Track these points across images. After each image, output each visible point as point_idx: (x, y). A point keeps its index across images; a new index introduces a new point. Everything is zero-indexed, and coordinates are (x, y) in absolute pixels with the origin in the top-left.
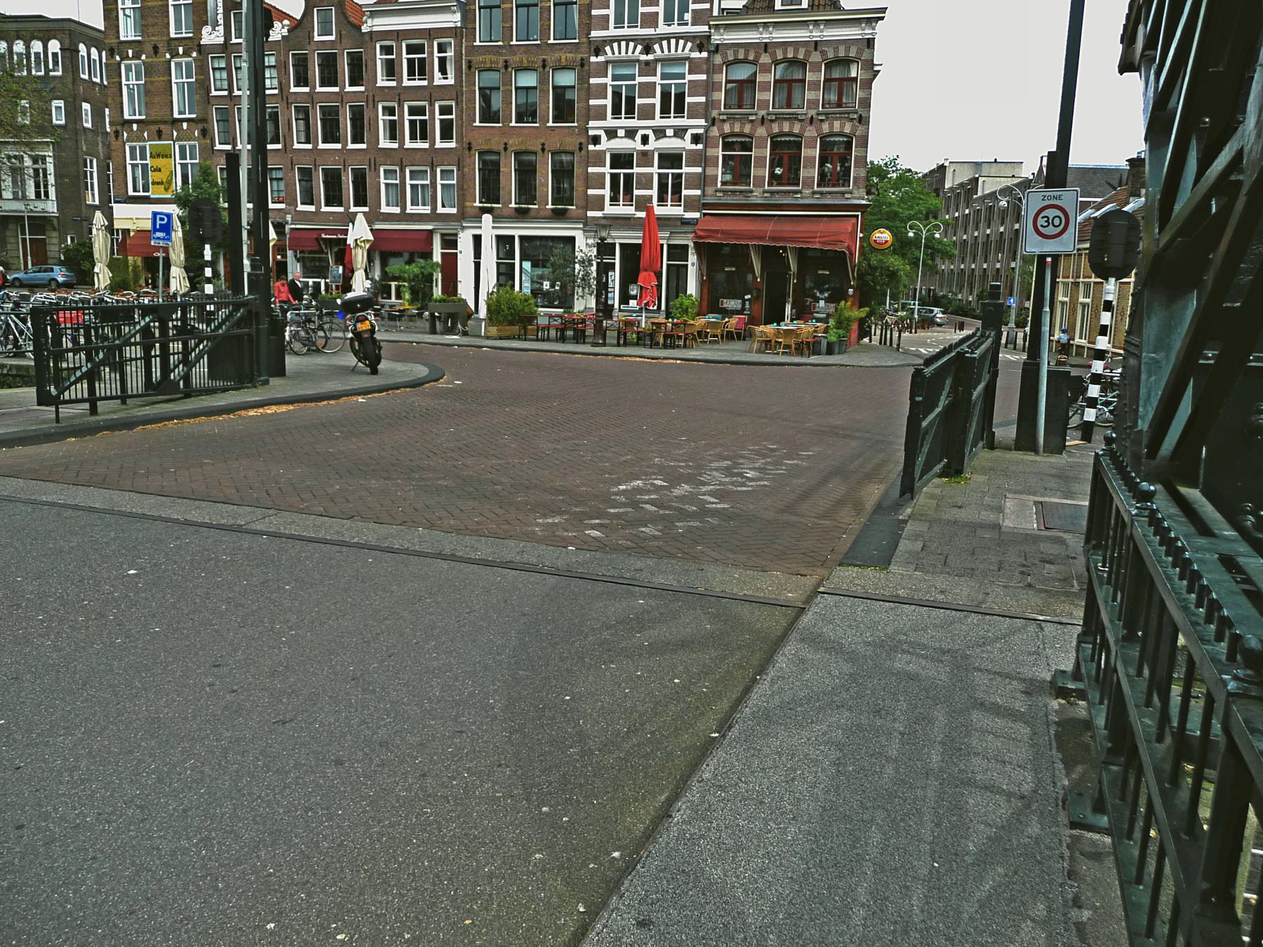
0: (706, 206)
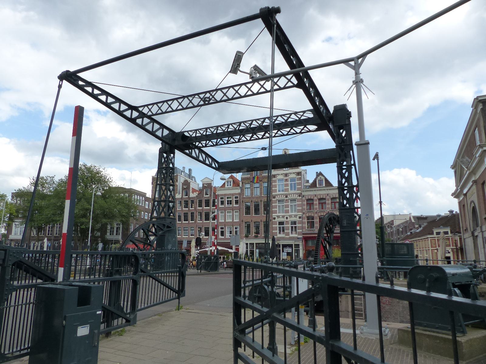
0: (303, 234)
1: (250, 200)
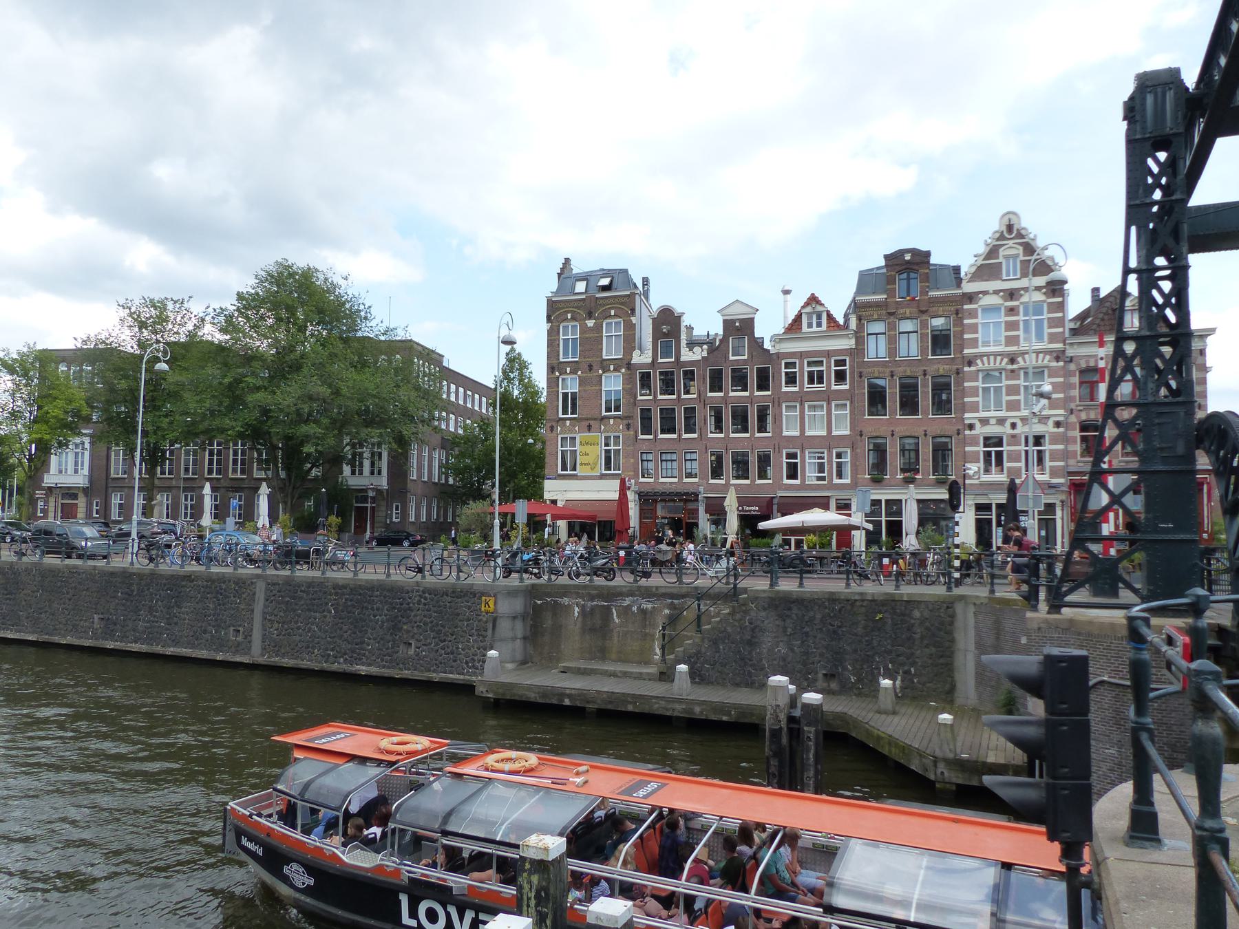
1: (888, 370)
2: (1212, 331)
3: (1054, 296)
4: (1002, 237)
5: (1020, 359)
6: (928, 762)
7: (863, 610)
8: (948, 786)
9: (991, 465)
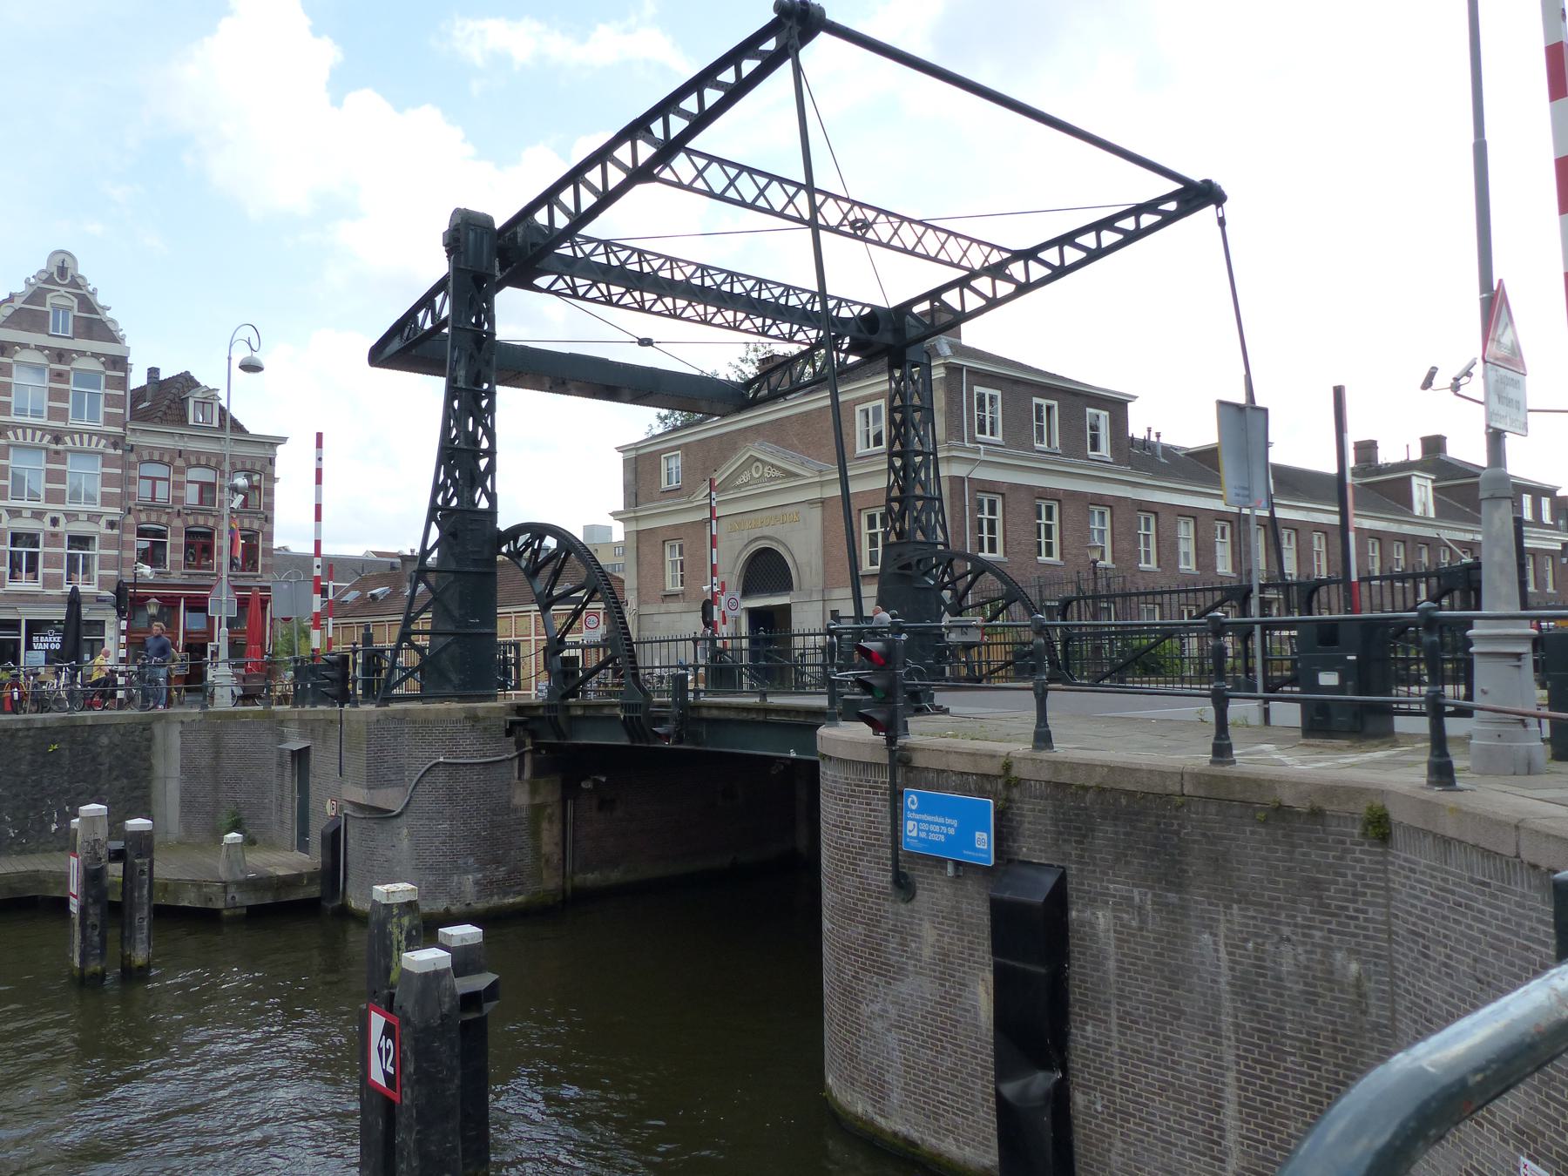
2: (283, 440)
3: (115, 369)
4: (50, 280)
5: (67, 439)
6: (216, 889)
7: (29, 741)
8: (238, 911)
9: (77, 572)
